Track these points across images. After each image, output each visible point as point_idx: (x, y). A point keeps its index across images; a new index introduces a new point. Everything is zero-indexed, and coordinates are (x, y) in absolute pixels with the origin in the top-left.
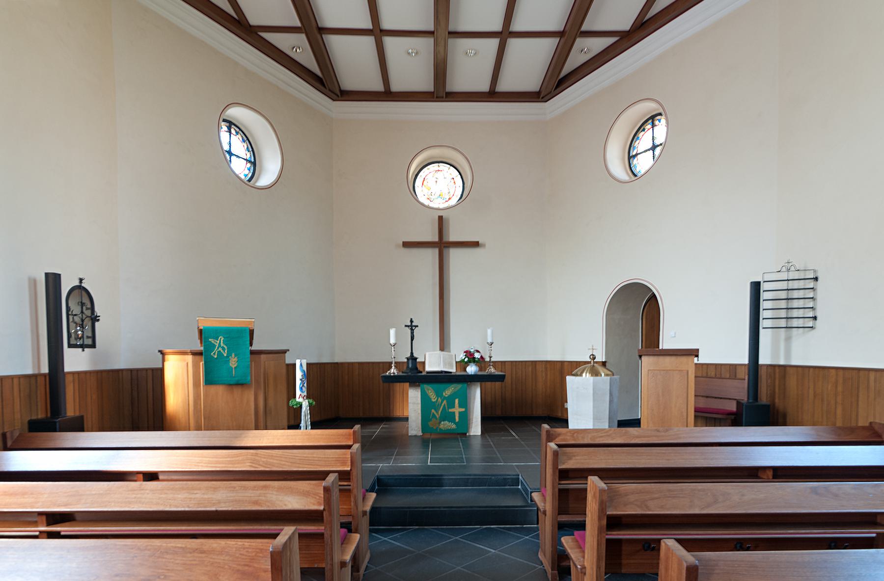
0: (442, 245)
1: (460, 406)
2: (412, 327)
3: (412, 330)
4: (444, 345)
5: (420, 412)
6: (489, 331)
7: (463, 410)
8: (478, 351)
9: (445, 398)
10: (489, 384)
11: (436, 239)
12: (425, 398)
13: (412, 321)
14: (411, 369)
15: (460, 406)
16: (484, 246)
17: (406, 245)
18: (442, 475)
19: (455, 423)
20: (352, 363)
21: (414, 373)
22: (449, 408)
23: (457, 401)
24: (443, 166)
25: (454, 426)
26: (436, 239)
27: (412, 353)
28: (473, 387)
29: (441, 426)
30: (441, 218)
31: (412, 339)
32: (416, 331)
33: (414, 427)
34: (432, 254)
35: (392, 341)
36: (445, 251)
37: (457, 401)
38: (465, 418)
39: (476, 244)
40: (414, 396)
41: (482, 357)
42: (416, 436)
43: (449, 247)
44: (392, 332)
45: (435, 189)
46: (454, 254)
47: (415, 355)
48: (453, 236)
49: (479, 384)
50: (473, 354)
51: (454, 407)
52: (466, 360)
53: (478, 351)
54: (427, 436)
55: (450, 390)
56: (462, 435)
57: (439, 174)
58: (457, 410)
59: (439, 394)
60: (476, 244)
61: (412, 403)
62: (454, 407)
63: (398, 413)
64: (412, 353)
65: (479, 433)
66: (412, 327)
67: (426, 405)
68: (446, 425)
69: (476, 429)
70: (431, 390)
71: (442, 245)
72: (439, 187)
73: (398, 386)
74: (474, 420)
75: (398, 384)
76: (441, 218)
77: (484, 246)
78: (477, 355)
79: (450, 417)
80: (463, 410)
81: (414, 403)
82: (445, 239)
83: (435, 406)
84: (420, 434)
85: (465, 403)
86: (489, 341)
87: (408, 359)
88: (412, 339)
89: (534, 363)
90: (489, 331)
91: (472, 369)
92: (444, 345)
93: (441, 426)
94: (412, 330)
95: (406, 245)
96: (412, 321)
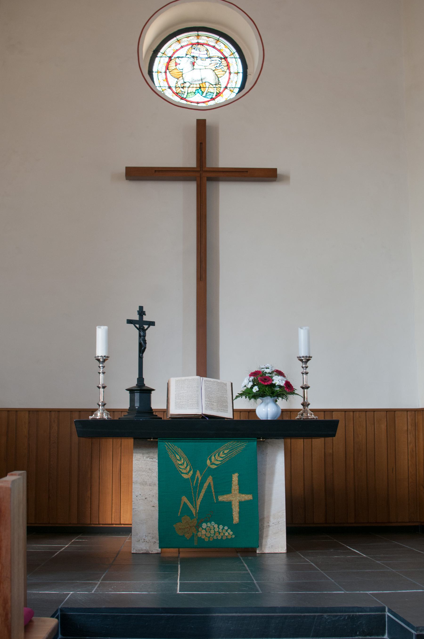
0: (204, 175)
1: (241, 491)
2: (142, 324)
3: (142, 332)
4: (205, 365)
5: (156, 501)
6: (302, 334)
7: (249, 497)
8: (280, 373)
9: (211, 471)
10: (299, 443)
11: (192, 163)
12: (167, 476)
13: (141, 312)
14: (139, 412)
15: (241, 491)
16: (285, 178)
17: (135, 174)
18: (208, 610)
19: (232, 527)
20: (17, 411)
21: (144, 424)
22: (219, 492)
23: (235, 478)
24: (205, 38)
25: (229, 533)
26: (192, 163)
27: (141, 379)
28: (269, 450)
29: (202, 533)
30: (201, 125)
31: (142, 348)
32: (150, 332)
33: (145, 537)
34: (183, 194)
35: (101, 351)
36: (210, 186)
37: (235, 478)
38: (253, 516)
39: (269, 175)
40: (144, 468)
41: (288, 384)
42: (147, 554)
43: (216, 179)
44: (101, 333)
45: (191, 76)
46: (229, 197)
47: (148, 384)
48: (226, 157)
49: (281, 443)
50: (270, 379)
51: (229, 491)
52: (256, 389)
53: (280, 373)
54: (171, 552)
55: (220, 454)
56: (247, 551)
57: (200, 52)
58: (235, 498)
59: (196, 463)
60: (269, 175)
61: (138, 488)
62: (229, 491)
63: (108, 518)
64: (141, 379)
65: (284, 550)
66: (142, 324)
67: (169, 485)
68: (213, 531)
69: (275, 540)
70: (179, 454)
71: (204, 175)
72: (198, 72)
73: (110, 444)
74: (272, 521)
75: (110, 441)
76: (201, 125)
77: (285, 178)
78: (278, 380)
79: (222, 514)
80: (249, 497)
81: (144, 483)
82: (210, 164)
83: (189, 488)
84: (156, 549)
85: (254, 483)
86: (303, 353)
87: (131, 391)
88: (142, 348)
89: (391, 414)
90: (302, 334)
91: (266, 410)
92: (205, 365)
93: (202, 533)
94: (142, 332)
95: (135, 174)
96: (141, 312)
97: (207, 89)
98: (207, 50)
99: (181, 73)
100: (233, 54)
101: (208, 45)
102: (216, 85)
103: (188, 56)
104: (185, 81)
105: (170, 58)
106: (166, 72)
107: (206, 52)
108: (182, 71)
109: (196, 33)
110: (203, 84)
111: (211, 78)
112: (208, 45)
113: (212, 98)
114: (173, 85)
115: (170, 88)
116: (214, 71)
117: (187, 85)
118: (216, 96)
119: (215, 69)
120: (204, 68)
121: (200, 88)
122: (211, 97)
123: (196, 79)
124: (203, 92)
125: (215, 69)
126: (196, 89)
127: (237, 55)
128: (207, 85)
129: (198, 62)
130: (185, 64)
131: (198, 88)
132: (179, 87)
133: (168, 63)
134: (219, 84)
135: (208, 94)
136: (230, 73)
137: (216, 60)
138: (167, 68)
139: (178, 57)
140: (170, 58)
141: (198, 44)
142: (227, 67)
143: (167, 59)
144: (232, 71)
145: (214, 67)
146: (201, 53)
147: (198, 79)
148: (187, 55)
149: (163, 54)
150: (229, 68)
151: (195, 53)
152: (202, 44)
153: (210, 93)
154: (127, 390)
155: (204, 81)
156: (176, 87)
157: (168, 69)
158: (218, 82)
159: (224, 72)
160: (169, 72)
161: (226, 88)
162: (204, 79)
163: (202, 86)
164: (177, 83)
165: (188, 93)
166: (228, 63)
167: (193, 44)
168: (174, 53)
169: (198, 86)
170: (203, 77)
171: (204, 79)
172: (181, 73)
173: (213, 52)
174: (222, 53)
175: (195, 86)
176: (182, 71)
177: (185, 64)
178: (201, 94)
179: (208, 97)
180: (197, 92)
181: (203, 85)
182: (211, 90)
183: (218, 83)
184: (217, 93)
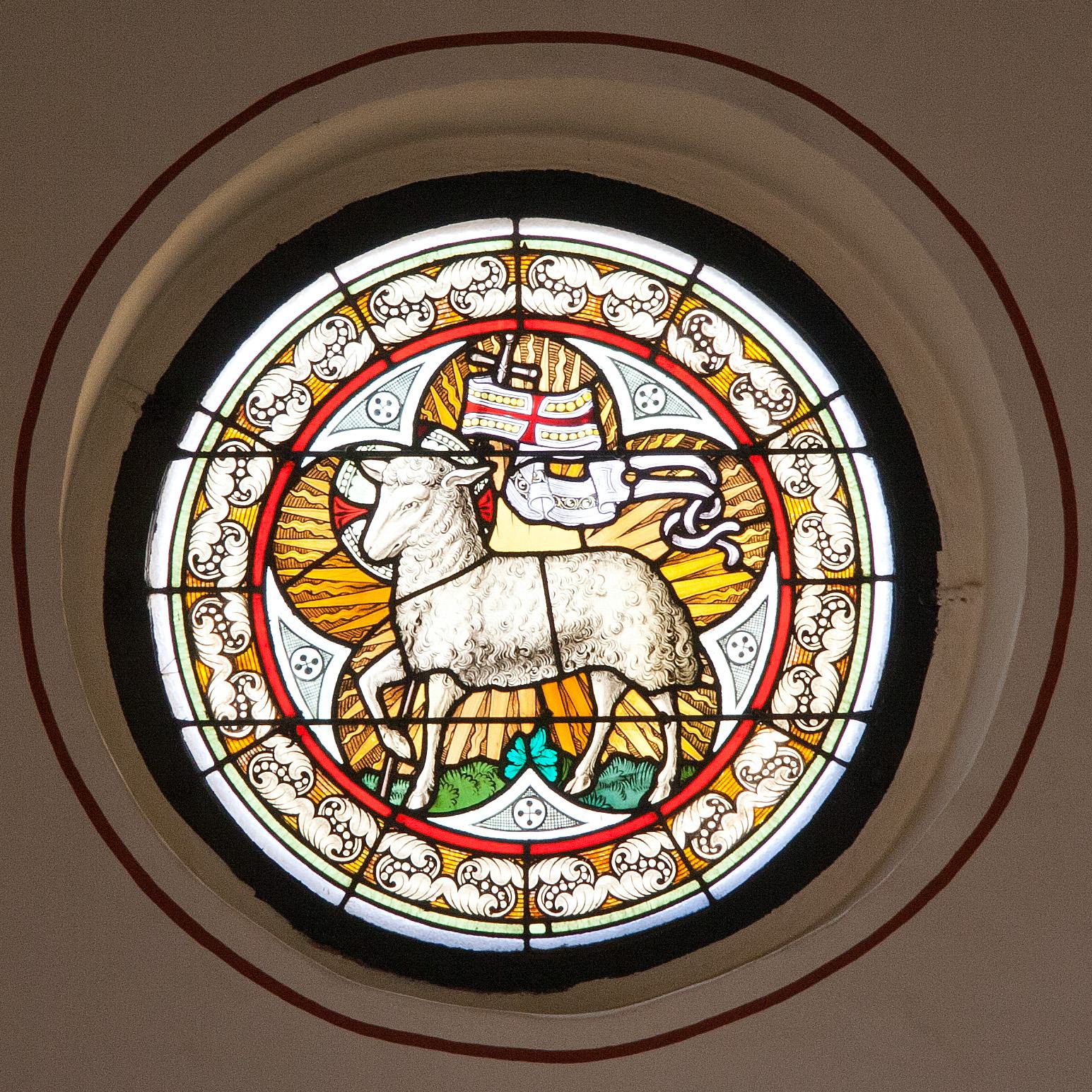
97: (601, 728)
98: (597, 383)
99: (383, 595)
100: (814, 413)
101: (609, 335)
102: (673, 690)
103: (436, 441)
104: (421, 661)
105: (289, 459)
106: (252, 589)
107: (582, 402)
108: (385, 573)
109: (503, 227)
110: (571, 685)
111: (620, 616)
112: (609, 335)
113: (644, 806)
114: (314, 699)
115: (291, 724)
116: (655, 566)
117: (440, 694)
118: (677, 785)
119: (660, 549)
120: (573, 541)
121: (544, 720)
122: (633, 799)
123: (503, 641)
124: (566, 764)
125: (660, 549)
126: (512, 729)
127: (846, 423)
128: (604, 689)
129: (533, 491)
130: (410, 512)
131: (527, 728)
132: (372, 723)
133: (272, 505)
134: (698, 685)
135: (609, 776)
136: (792, 584)
137: (671, 474)
138: (264, 552)
139: (351, 454)
140: (289, 459)
141: (521, 322)
142: (548, 266)
143: (260, 471)
144: (808, 562)
145: (653, 531)
146: (547, 408)
147: (530, 644)
148: (423, 427)
149: (230, 422)
150: (781, 542)
151: (500, 411)
152: (556, 330)
153: (625, 768)
154: (229, 601)
155: (574, 658)
156: (337, 723)
157: (270, 561)
158: (689, 671)
159: (744, 576)
160: (283, 586)
161: (759, 715)
162: (577, 640)
163: (557, 709)
164: (349, 677)
165: (441, 770)
166: (773, 492)
167: (471, 333)
168: (318, 416)
169: (527, 704)
170: (566, 620)
171: (577, 640)
172: (383, 595)
173: (650, 403)
174: (724, 410)
175: (500, 705)
176: (385, 573)
177: (410, 512)
178: (552, 775)
179: (612, 796)
180: (516, 757)
181: (566, 700)
182: (641, 741)
183: (695, 675)
184: (682, 762)
